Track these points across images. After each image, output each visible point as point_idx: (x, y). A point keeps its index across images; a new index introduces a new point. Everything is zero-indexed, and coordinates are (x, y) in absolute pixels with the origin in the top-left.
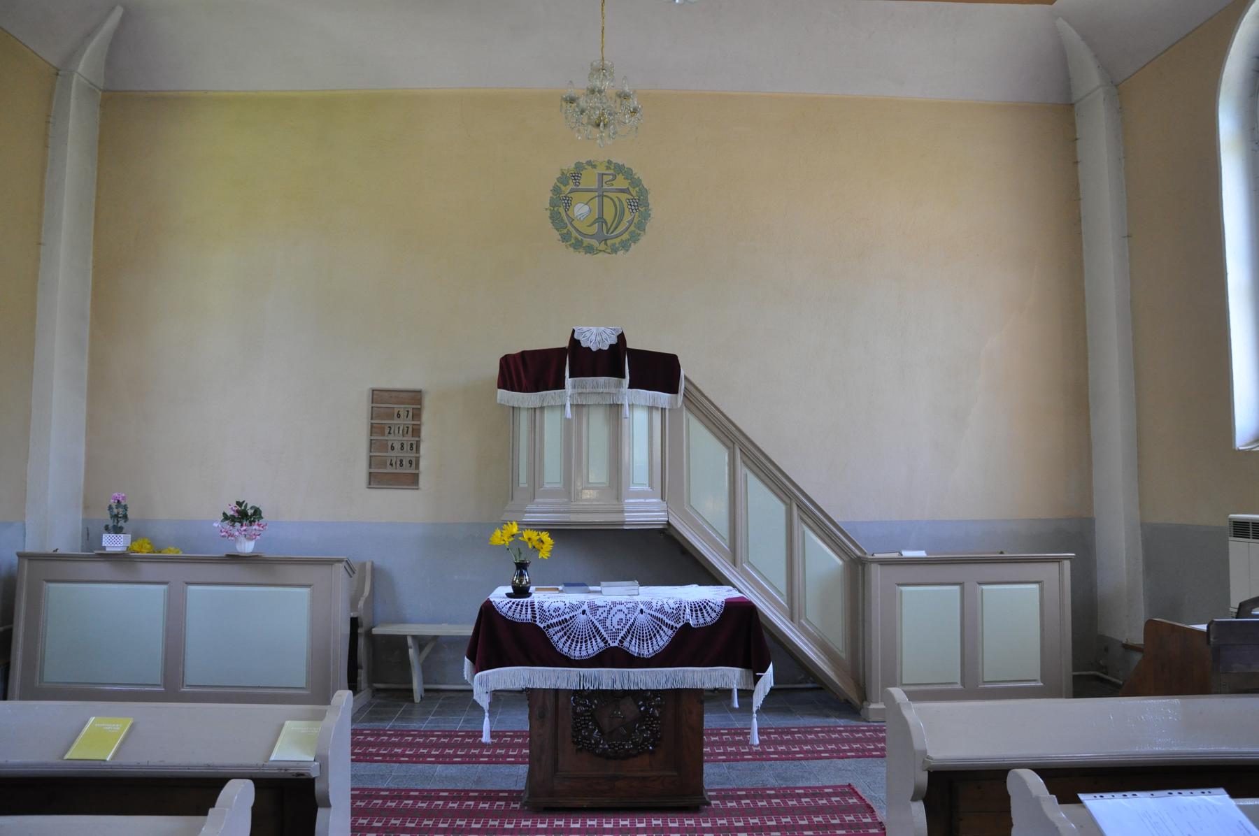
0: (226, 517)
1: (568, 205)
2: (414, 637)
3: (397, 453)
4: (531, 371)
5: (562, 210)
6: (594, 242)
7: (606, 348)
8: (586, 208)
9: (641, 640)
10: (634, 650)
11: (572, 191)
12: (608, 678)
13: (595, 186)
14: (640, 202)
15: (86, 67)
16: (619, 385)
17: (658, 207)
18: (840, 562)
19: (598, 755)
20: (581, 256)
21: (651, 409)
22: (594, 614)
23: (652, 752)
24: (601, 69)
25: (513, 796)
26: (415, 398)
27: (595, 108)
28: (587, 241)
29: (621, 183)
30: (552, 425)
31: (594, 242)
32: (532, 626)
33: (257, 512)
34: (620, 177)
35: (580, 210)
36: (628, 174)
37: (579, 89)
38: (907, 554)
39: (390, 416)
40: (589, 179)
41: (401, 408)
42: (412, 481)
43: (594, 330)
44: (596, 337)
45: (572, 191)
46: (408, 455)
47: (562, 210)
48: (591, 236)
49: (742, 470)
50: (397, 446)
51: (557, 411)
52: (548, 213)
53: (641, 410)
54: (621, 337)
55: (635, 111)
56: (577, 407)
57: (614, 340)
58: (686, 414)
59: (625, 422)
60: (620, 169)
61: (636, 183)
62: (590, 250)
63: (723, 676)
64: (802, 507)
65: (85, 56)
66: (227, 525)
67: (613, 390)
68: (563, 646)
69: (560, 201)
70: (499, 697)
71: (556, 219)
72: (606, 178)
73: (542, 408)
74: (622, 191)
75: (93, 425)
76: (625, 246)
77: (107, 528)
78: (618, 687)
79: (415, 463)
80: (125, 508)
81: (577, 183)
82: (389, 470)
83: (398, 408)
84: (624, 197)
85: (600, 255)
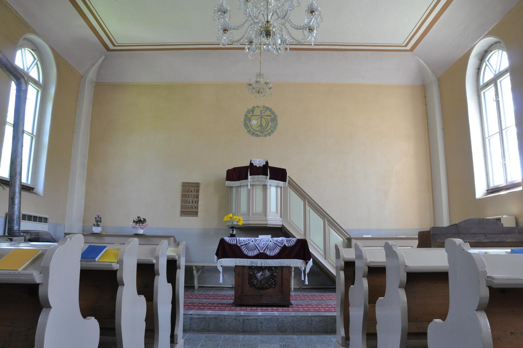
0: (134, 221)
1: (250, 120)
2: (196, 266)
3: (191, 204)
4: (237, 174)
5: (248, 122)
6: (259, 133)
7: (262, 166)
8: (256, 122)
9: (270, 250)
10: (268, 253)
11: (251, 116)
12: (260, 262)
13: (259, 114)
14: (274, 120)
15: (91, 75)
16: (266, 178)
17: (280, 121)
18: (342, 240)
19: (257, 288)
20: (254, 138)
21: (277, 187)
22: (256, 242)
23: (274, 288)
24: (260, 75)
25: (230, 304)
26: (197, 185)
27: (257, 88)
28: (256, 133)
29: (268, 113)
30: (244, 192)
31: (259, 133)
32: (236, 245)
33: (145, 220)
34: (268, 111)
35: (254, 122)
36: (270, 110)
37: (253, 81)
38: (364, 236)
39: (189, 191)
40: (257, 112)
41: (192, 189)
42: (196, 214)
43: (258, 160)
44: (259, 162)
45: (251, 116)
46: (194, 205)
47: (248, 122)
48: (258, 131)
49: (308, 208)
50: (191, 202)
51: (247, 189)
52: (243, 123)
53: (274, 188)
54: (267, 162)
55: (270, 88)
56: (252, 185)
57: (264, 164)
58: (289, 189)
59: (268, 190)
60: (267, 108)
61: (273, 113)
62: (257, 136)
63: (296, 262)
64: (330, 222)
65: (92, 70)
66: (134, 224)
67: (264, 180)
68: (246, 252)
69: (247, 120)
70: (226, 269)
71: (246, 125)
72: (263, 112)
73: (240, 186)
74: (268, 116)
75: (87, 193)
76: (269, 134)
77: (94, 225)
78: (263, 265)
79: (197, 208)
80: (101, 218)
81: (253, 113)
82: (188, 210)
83: (192, 189)
84: (269, 118)
85: (261, 137)
